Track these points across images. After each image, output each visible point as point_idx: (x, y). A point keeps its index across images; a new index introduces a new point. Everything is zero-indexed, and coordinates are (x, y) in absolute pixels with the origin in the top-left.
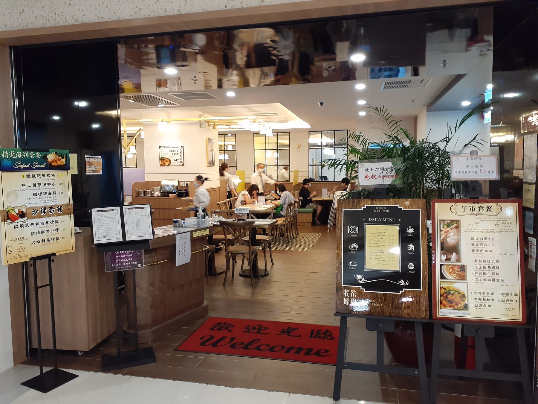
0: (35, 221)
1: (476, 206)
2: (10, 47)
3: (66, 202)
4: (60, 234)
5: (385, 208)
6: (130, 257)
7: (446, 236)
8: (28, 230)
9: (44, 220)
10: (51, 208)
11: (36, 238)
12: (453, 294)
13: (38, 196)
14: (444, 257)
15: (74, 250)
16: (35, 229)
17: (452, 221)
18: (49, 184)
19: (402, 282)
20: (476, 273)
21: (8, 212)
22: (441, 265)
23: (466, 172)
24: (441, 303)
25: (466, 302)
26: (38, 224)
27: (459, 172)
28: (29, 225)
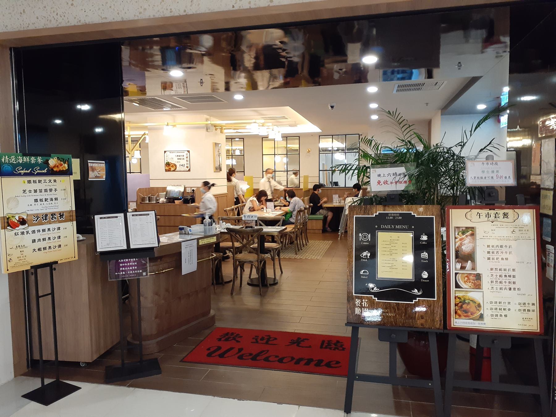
0: (36, 228)
1: (492, 212)
2: (10, 49)
3: (69, 209)
4: (62, 242)
5: (398, 215)
6: (135, 266)
7: (461, 244)
8: (29, 238)
9: (46, 227)
10: (53, 214)
11: (37, 245)
12: (469, 303)
13: (39, 203)
14: (459, 266)
15: (77, 258)
16: (37, 236)
17: (467, 228)
18: (51, 190)
19: (416, 291)
20: (492, 282)
21: (8, 219)
22: (456, 274)
23: (482, 178)
24: (456, 313)
25: (482, 312)
26: (39, 231)
27: (475, 178)
28: (30, 232)
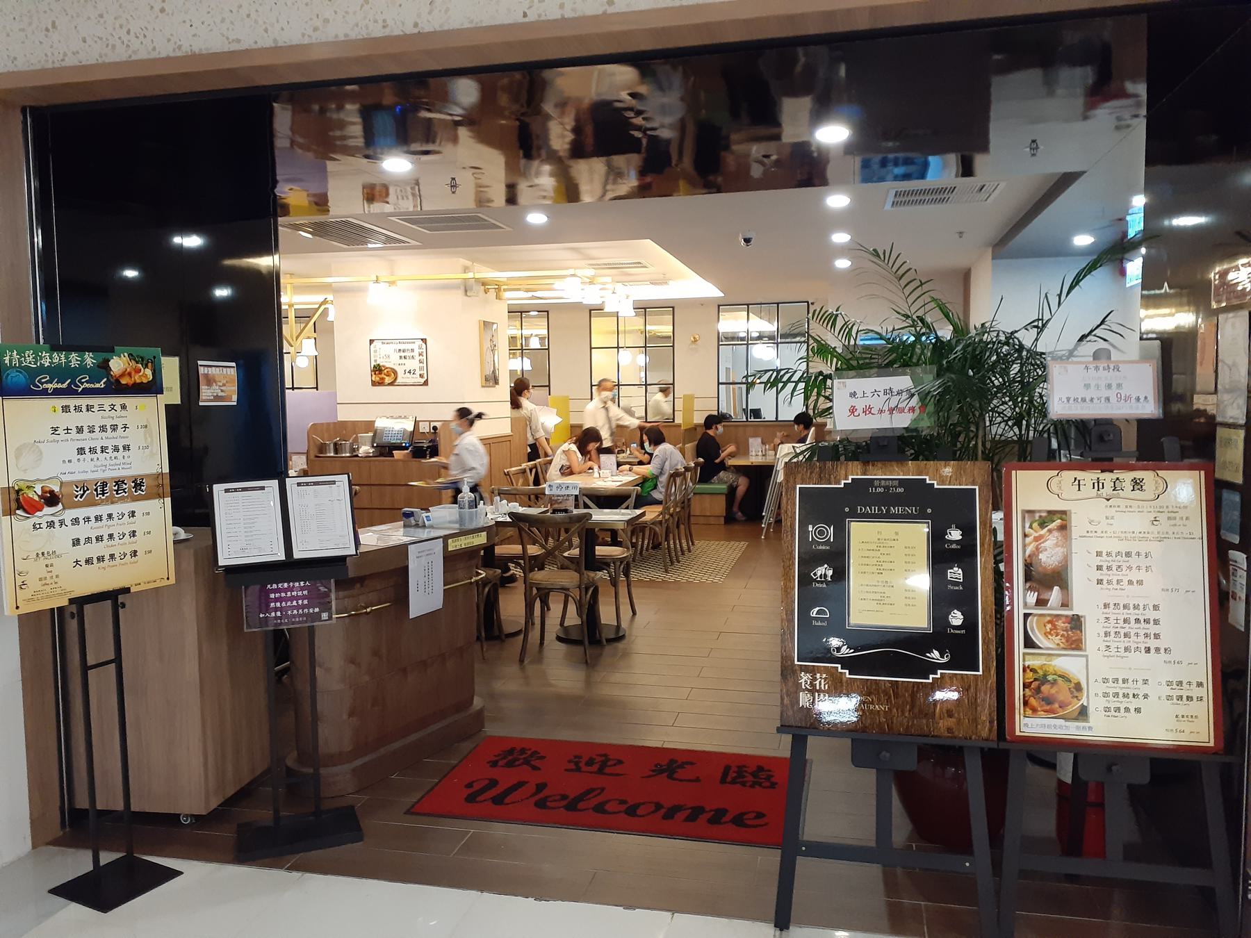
0: (81, 513)
1: (1108, 477)
2: (24, 110)
3: (154, 470)
4: (140, 543)
5: (896, 483)
6: (303, 597)
7: (1037, 548)
8: (64, 535)
9: (103, 510)
10: (119, 482)
11: (83, 552)
12: (1054, 683)
13: (88, 456)
14: (1032, 598)
15: (172, 581)
16: (82, 531)
17: (1051, 513)
18: (114, 428)
19: (936, 654)
20: (1106, 634)
21: (18, 492)
22: (1026, 616)
23: (1084, 400)
24: (1026, 703)
25: (1084, 701)
26: (87, 519)
27: (1068, 399)
28: (68, 522)
